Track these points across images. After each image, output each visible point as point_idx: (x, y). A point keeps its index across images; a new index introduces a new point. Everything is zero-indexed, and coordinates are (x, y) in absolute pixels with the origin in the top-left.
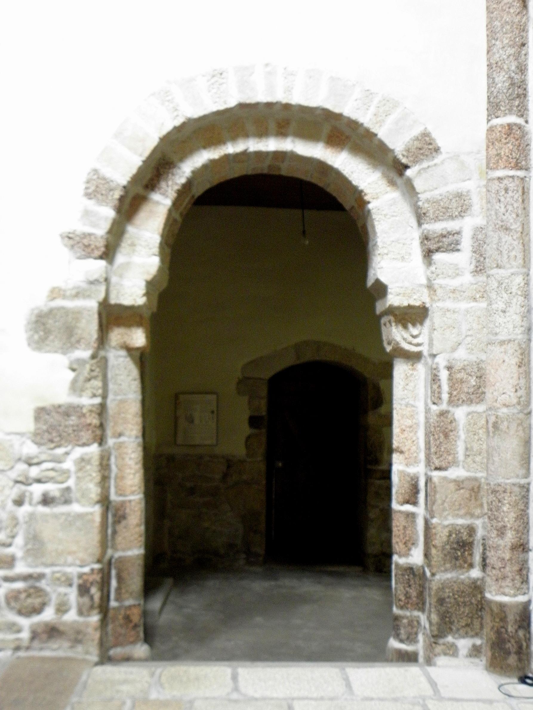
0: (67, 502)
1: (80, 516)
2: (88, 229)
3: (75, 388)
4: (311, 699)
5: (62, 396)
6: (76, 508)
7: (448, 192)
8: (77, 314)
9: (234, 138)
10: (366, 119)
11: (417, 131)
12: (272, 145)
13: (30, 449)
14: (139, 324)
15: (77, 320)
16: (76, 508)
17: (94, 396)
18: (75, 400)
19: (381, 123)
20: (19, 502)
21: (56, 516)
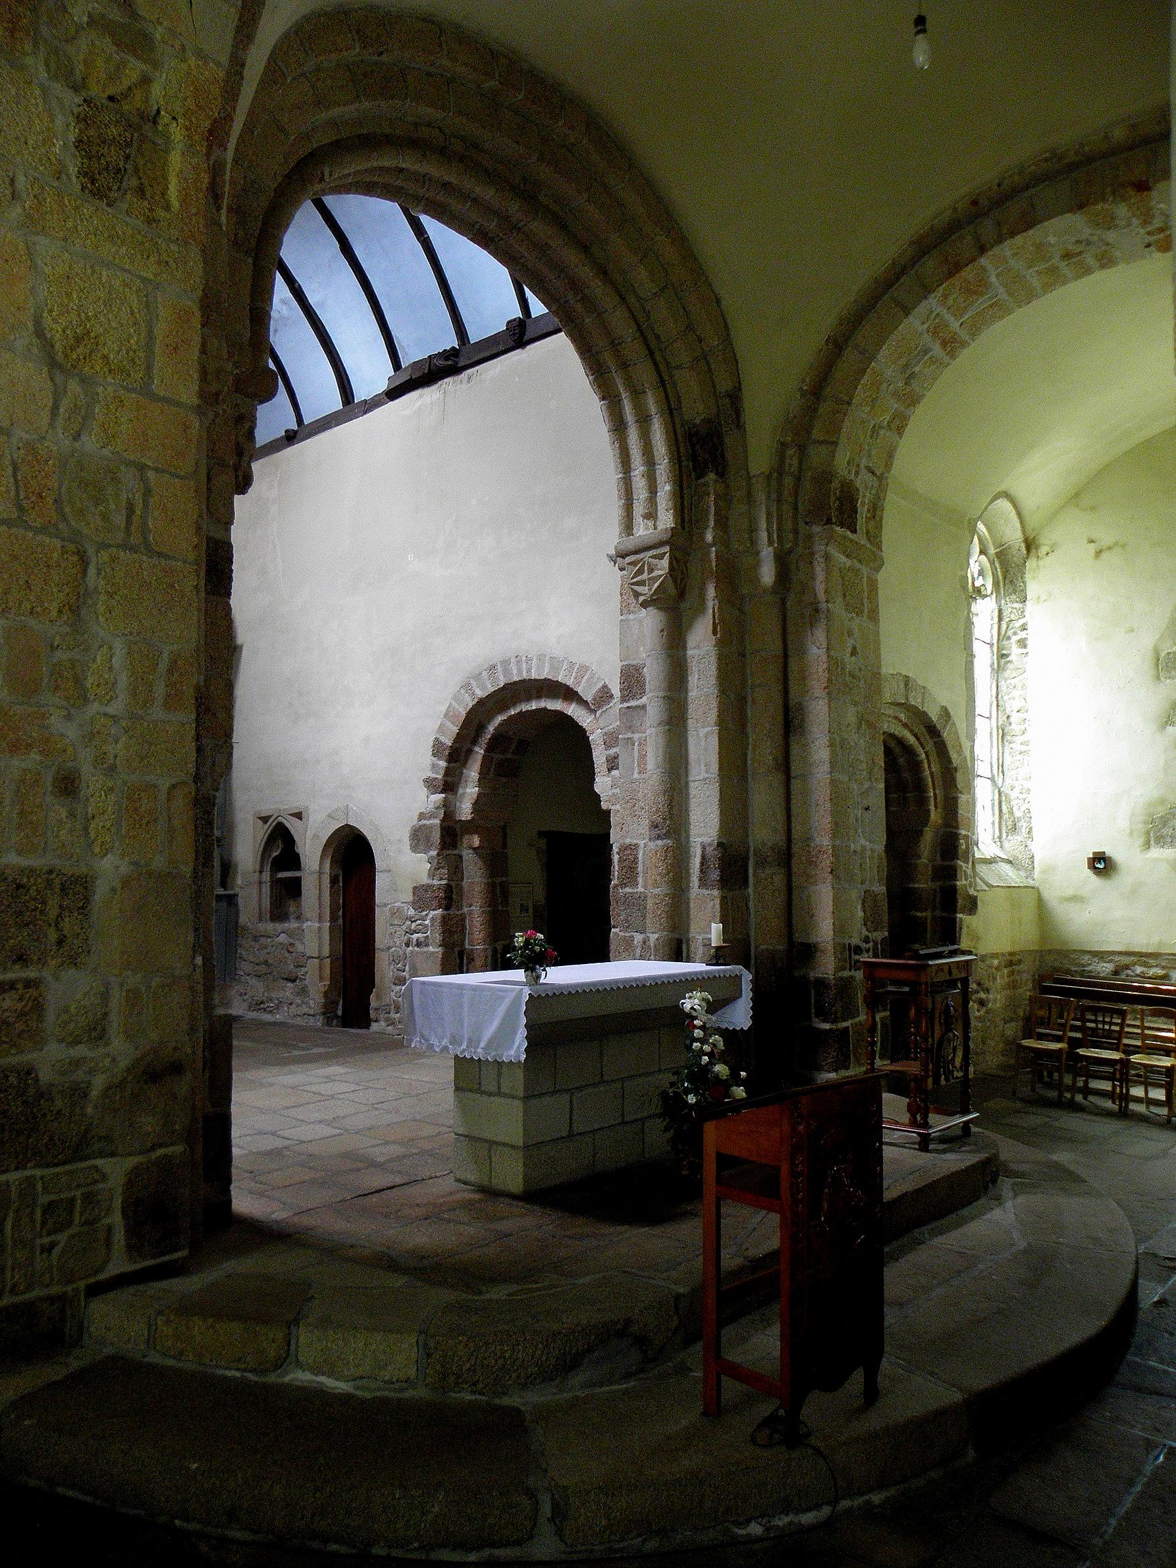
0: (427, 945)
1: (433, 953)
2: (434, 776)
3: (432, 875)
4: (571, 1111)
5: (425, 880)
6: (431, 949)
7: (907, 680)
8: (431, 827)
9: (514, 705)
10: (570, 682)
11: (600, 685)
12: (534, 705)
13: (411, 912)
14: (476, 832)
15: (431, 832)
16: (431, 949)
17: (441, 879)
18: (430, 882)
19: (579, 683)
20: (407, 945)
21: (422, 953)
